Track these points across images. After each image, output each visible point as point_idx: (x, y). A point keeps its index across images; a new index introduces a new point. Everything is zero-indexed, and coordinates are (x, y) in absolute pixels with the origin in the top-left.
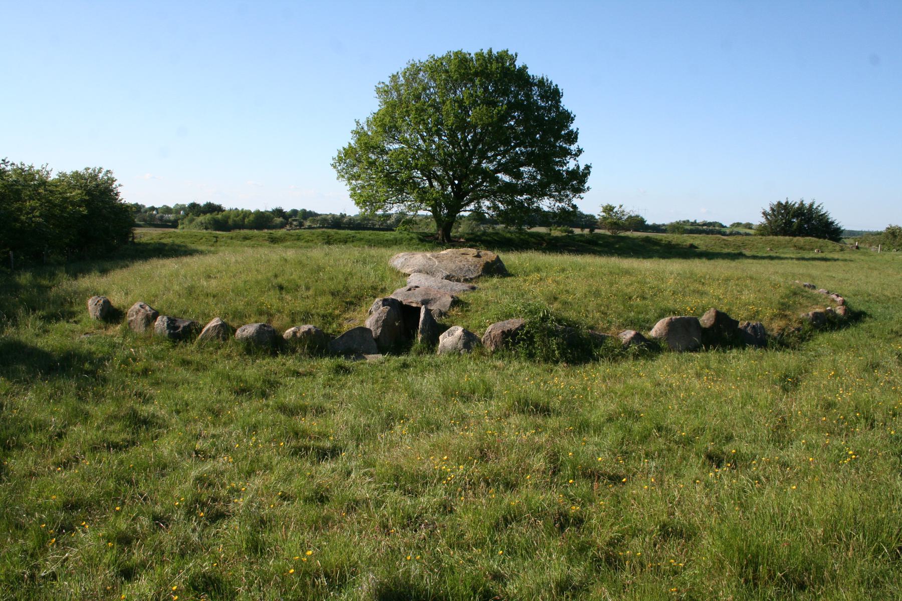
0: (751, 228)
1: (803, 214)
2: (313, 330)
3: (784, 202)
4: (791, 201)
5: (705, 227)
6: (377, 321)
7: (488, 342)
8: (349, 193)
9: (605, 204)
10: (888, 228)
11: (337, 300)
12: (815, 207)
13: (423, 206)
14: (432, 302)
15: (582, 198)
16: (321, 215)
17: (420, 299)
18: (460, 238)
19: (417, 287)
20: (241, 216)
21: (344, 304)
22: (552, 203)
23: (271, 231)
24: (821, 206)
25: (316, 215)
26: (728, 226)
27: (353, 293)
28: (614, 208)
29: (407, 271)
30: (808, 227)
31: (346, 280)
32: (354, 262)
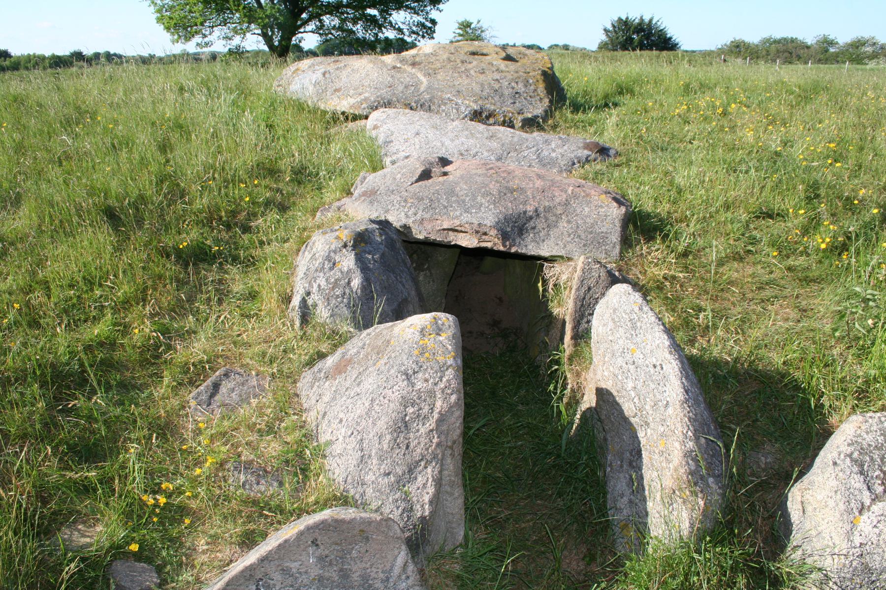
1: (642, 30)
3: (624, 19)
4: (632, 17)
6: (402, 426)
10: (732, 42)
12: (654, 22)
13: (253, 26)
14: (540, 224)
17: (489, 217)
21: (171, 268)
22: (408, 16)
24: (661, 21)
28: (471, 24)
29: (344, 105)
30: (648, 42)
31: (164, 147)
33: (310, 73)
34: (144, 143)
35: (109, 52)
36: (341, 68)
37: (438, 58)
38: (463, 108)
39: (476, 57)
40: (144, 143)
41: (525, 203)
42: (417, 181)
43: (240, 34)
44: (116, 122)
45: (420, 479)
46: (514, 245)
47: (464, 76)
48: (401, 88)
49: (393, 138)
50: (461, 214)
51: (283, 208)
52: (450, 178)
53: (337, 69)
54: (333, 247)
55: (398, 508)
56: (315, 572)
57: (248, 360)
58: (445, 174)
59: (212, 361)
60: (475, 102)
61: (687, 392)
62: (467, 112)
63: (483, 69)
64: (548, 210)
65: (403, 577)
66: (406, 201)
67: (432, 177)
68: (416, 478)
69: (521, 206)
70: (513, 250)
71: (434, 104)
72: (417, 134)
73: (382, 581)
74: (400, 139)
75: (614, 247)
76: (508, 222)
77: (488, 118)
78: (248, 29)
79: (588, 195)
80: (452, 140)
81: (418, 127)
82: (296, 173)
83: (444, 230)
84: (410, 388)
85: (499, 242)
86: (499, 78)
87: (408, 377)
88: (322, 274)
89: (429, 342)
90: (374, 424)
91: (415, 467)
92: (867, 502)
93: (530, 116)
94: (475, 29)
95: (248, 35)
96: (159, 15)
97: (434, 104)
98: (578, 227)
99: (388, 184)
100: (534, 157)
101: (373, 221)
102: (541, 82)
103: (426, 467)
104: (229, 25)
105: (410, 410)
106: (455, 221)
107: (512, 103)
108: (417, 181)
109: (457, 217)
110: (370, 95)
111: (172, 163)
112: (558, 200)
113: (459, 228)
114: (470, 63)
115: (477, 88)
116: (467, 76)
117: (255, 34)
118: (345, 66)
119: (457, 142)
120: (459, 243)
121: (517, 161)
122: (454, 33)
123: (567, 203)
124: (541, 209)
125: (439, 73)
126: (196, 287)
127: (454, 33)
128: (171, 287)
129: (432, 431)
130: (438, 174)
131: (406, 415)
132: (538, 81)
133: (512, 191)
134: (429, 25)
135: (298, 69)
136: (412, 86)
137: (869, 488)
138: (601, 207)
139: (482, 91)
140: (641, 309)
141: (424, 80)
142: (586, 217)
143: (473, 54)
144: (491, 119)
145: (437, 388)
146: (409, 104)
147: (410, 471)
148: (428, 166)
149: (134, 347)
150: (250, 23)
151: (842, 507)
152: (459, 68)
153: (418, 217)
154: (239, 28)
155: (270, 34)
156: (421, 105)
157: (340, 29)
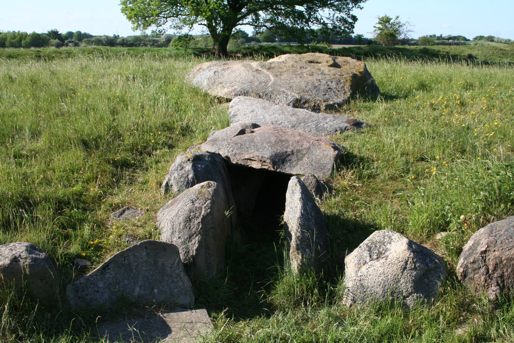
0: (492, 41)
2: (25, 262)
5: (451, 41)
6: (188, 220)
7: (480, 277)
8: (121, 6)
9: (382, 15)
11: (94, 161)
13: (199, 18)
14: (294, 158)
15: (361, 9)
16: (96, 36)
17: (267, 153)
18: (236, 53)
19: (255, 126)
20: (18, 37)
21: (109, 168)
22: (332, 12)
23: (38, 49)
25: (91, 36)
26: (471, 39)
27: (129, 140)
28: (390, 19)
29: (221, 92)
32: (128, 79)
33: (207, 71)
34: (102, 109)
35: (80, 32)
36: (225, 69)
37: (286, 65)
38: (290, 97)
39: (312, 64)
40: (102, 109)
41: (287, 147)
42: (237, 135)
43: (189, 24)
44: (88, 97)
45: (193, 241)
46: (279, 168)
47: (298, 77)
48: (256, 83)
49: (238, 113)
50: (254, 152)
51: (171, 147)
52: (254, 134)
53: (223, 70)
54: (183, 161)
55: (183, 251)
56: (145, 258)
57: (138, 204)
58: (252, 132)
59: (123, 203)
60: (299, 93)
61: (302, 215)
62: (292, 100)
63: (312, 73)
64: (298, 151)
65: (178, 268)
66: (229, 144)
67: (245, 133)
68: (192, 241)
69: (285, 149)
70: (278, 170)
71: (273, 94)
72: (253, 111)
73: (170, 268)
74: (242, 114)
75: (328, 171)
76: (277, 157)
77: (304, 103)
78: (195, 21)
79: (320, 145)
80: (270, 116)
81: (254, 107)
82: (183, 130)
83: (245, 159)
84: (193, 206)
85: (271, 166)
86: (320, 78)
87: (193, 202)
88: (176, 172)
89: (204, 190)
90: (178, 219)
91: (192, 236)
92: (368, 261)
93: (331, 103)
94: (393, 24)
95: (195, 25)
96: (124, 6)
97: (273, 94)
98: (312, 160)
99: (223, 136)
100: (314, 126)
101: (208, 152)
102: (349, 81)
103: (196, 237)
104: (180, 16)
105: (192, 214)
106: (251, 155)
107: (323, 95)
108: (237, 135)
109: (252, 153)
110: (237, 87)
111: (117, 121)
112: (304, 147)
113: (252, 159)
114: (306, 68)
115: (303, 85)
116: (301, 77)
117: (201, 24)
118: (228, 68)
119: (273, 116)
120: (252, 166)
121: (303, 128)
122: (375, 27)
123: (309, 149)
124: (295, 151)
125: (283, 74)
126: (120, 177)
127: (375, 27)
128: (109, 176)
129: (199, 222)
130: (249, 132)
131: (190, 216)
132: (347, 81)
133: (282, 141)
134: (350, 20)
135: (200, 69)
136: (264, 82)
137: (370, 256)
138: (326, 151)
139: (306, 87)
140: (296, 185)
141: (272, 78)
142: (317, 155)
143: (311, 62)
144: (306, 104)
145: (203, 206)
146: (259, 94)
147: (190, 237)
148: (244, 128)
149: (90, 196)
150: (197, 16)
151: (356, 262)
152: (298, 71)
153: (234, 152)
154: (187, 19)
155: (214, 25)
156: (266, 95)
157: (272, 21)
